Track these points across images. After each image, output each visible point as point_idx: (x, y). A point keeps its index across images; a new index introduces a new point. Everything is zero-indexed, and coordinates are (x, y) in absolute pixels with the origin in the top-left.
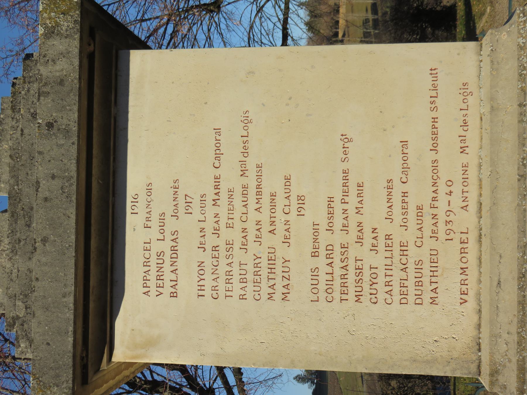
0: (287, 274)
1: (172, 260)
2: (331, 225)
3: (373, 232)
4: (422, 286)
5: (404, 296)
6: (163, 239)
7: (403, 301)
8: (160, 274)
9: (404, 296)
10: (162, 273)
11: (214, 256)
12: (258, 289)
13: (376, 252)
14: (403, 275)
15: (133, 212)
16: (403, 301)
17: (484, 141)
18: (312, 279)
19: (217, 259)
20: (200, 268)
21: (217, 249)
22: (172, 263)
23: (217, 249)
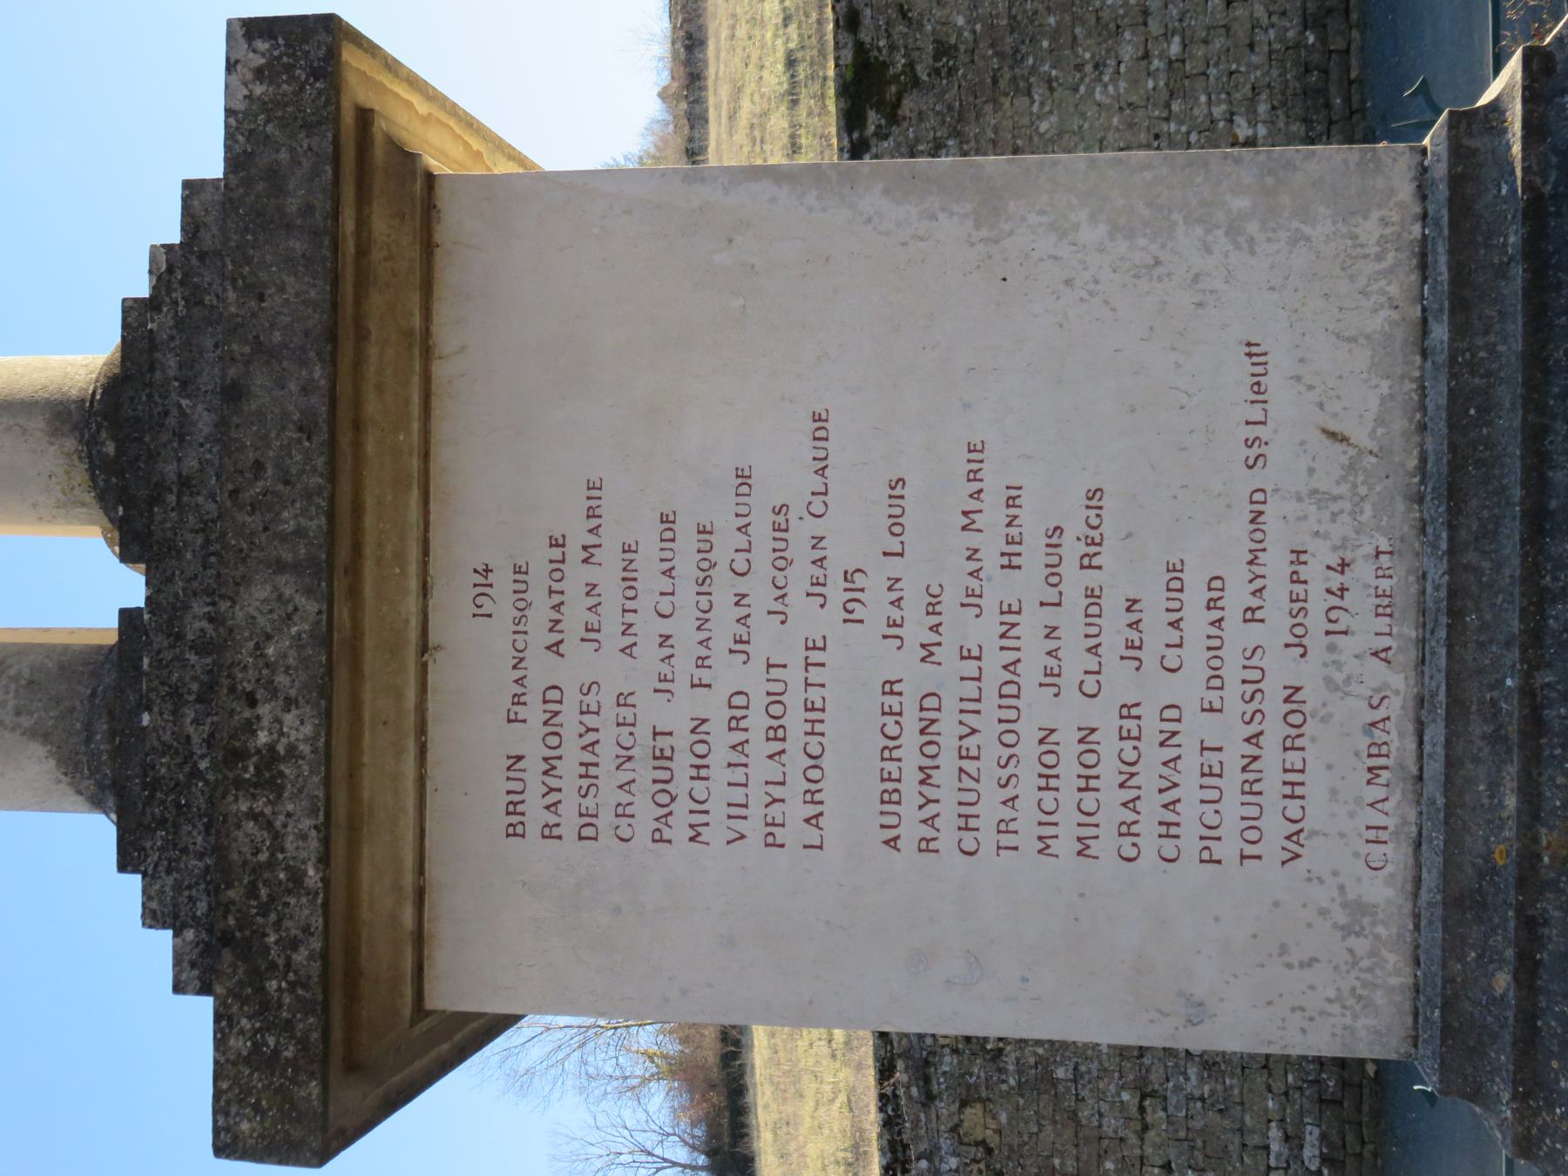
0: (975, 763)
1: (926, 714)
2: (1299, 631)
3: (1128, 610)
4: (898, 803)
5: (588, 820)
6: (1096, 668)
7: (587, 832)
8: (1251, 776)
9: (588, 820)
10: (1258, 776)
11: (1125, 734)
12: (1214, 795)
13: (744, 657)
14: (773, 771)
15: (1332, 627)
16: (587, 832)
17: (1424, 896)
18: (1202, 787)
19: (1135, 743)
20: (1045, 748)
21: (1134, 711)
22: (925, 723)
23: (1134, 711)
